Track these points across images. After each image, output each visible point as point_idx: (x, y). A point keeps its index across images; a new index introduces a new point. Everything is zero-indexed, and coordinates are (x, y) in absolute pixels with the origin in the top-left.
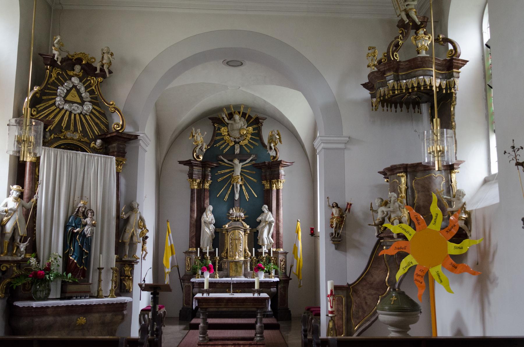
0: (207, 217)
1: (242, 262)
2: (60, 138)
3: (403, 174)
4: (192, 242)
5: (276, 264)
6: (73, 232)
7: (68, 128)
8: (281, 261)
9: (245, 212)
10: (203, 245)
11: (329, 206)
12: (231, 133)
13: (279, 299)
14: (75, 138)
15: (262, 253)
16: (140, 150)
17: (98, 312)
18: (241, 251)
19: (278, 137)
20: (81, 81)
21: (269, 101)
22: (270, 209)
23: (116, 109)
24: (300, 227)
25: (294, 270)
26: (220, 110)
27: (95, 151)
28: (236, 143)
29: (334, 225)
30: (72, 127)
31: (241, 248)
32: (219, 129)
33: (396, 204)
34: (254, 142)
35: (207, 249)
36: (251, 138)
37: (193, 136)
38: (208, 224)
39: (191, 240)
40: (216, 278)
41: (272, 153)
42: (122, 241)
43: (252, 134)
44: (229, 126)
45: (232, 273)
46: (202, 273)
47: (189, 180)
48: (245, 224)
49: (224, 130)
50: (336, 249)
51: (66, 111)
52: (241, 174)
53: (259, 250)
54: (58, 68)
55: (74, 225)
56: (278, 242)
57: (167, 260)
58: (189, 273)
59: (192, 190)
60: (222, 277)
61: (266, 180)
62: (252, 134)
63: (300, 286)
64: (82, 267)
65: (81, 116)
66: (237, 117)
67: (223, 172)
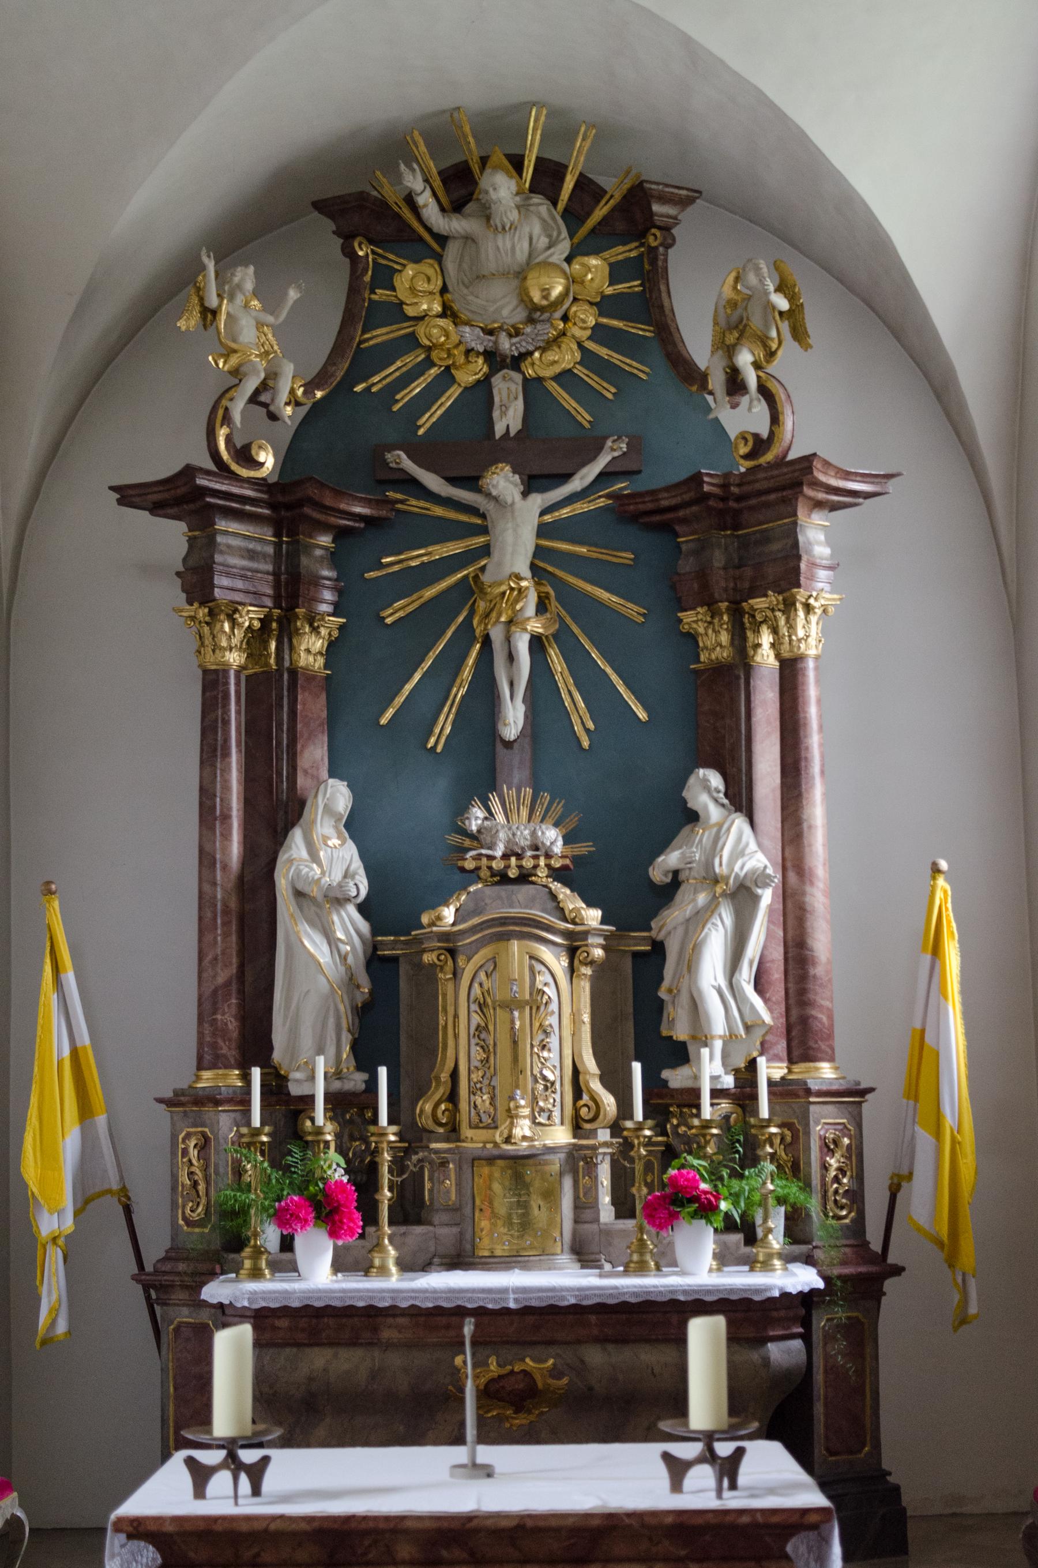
0: (314, 857)
1: (556, 1163)
4: (220, 1031)
5: (794, 1168)
8: (828, 1147)
9: (573, 821)
10: (292, 1049)
12: (464, 300)
13: (819, 1409)
15: (696, 1093)
18: (549, 1085)
19: (782, 303)
21: (718, 40)
22: (740, 798)
24: (949, 915)
25: (921, 1205)
26: (392, 148)
28: (495, 360)
31: (552, 1063)
32: (385, 277)
34: (616, 358)
35: (317, 1070)
36: (599, 333)
37: (209, 314)
38: (318, 903)
39: (207, 1007)
40: (383, 1271)
41: (745, 418)
43: (604, 305)
44: (452, 251)
45: (491, 1235)
46: (287, 1244)
47: (189, 610)
48: (571, 900)
49: (415, 285)
52: (533, 567)
53: (676, 1078)
56: (805, 1021)
57: (49, 1155)
58: (196, 1237)
59: (213, 682)
60: (425, 1267)
61: (710, 603)
62: (604, 305)
63: (963, 1320)
66: (502, 189)
67: (418, 557)
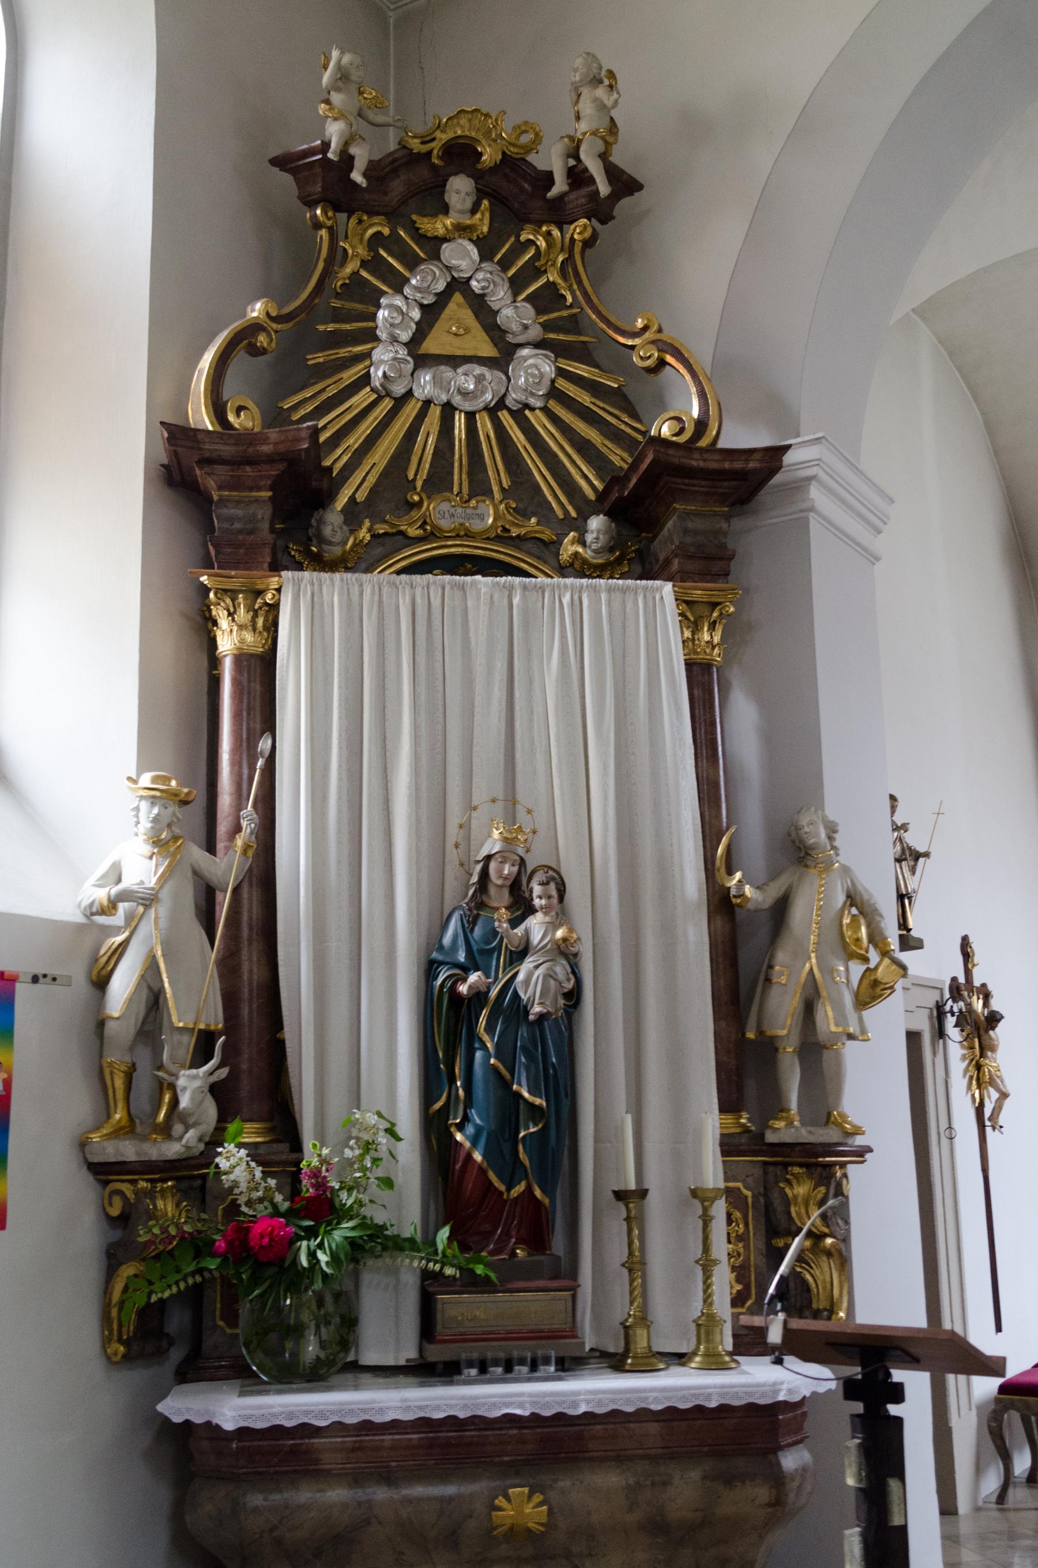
2: (402, 533)
6: (455, 998)
7: (439, 481)
14: (477, 526)
16: (821, 545)
17: (620, 1459)
20: (486, 255)
23: (666, 347)
27: (580, 568)
30: (459, 477)
42: (760, 1033)
51: (427, 403)
54: (371, 213)
55: (461, 957)
56: (401, 1249)
64: (520, 1188)
65: (504, 416)
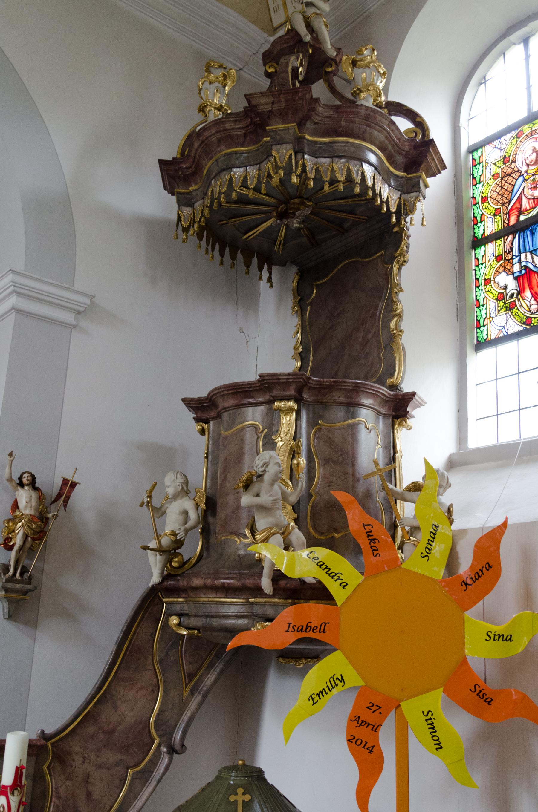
3: (291, 404)
11: (10, 480)
29: (18, 541)
33: (276, 487)
50: (11, 616)
